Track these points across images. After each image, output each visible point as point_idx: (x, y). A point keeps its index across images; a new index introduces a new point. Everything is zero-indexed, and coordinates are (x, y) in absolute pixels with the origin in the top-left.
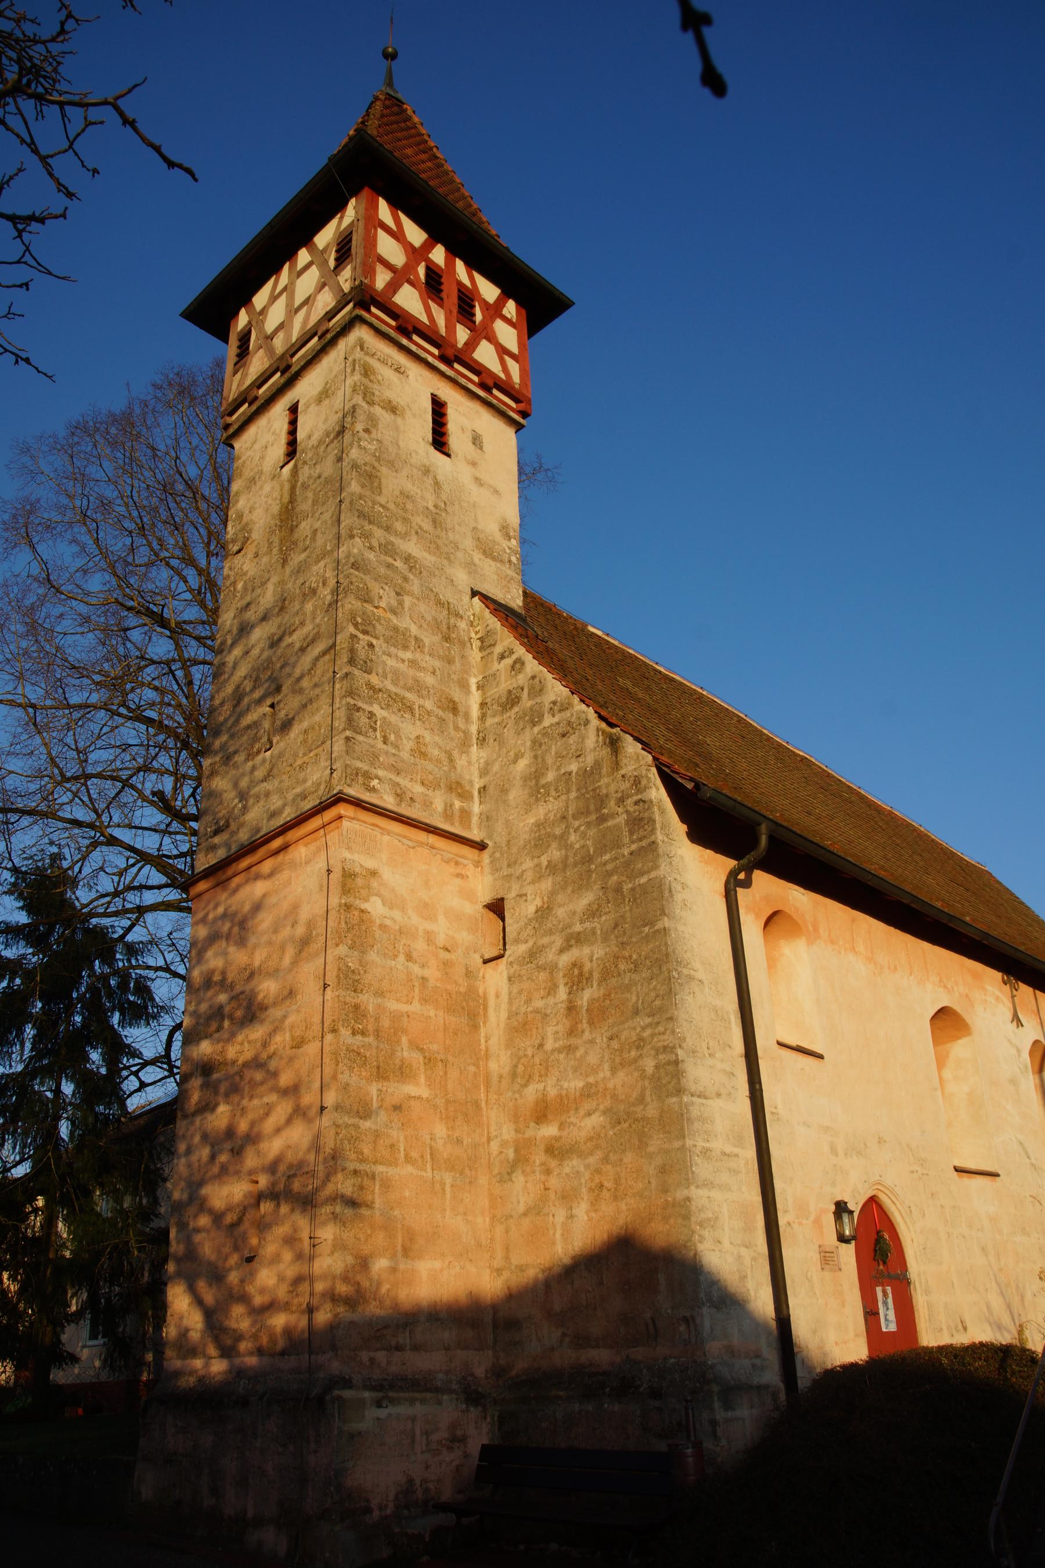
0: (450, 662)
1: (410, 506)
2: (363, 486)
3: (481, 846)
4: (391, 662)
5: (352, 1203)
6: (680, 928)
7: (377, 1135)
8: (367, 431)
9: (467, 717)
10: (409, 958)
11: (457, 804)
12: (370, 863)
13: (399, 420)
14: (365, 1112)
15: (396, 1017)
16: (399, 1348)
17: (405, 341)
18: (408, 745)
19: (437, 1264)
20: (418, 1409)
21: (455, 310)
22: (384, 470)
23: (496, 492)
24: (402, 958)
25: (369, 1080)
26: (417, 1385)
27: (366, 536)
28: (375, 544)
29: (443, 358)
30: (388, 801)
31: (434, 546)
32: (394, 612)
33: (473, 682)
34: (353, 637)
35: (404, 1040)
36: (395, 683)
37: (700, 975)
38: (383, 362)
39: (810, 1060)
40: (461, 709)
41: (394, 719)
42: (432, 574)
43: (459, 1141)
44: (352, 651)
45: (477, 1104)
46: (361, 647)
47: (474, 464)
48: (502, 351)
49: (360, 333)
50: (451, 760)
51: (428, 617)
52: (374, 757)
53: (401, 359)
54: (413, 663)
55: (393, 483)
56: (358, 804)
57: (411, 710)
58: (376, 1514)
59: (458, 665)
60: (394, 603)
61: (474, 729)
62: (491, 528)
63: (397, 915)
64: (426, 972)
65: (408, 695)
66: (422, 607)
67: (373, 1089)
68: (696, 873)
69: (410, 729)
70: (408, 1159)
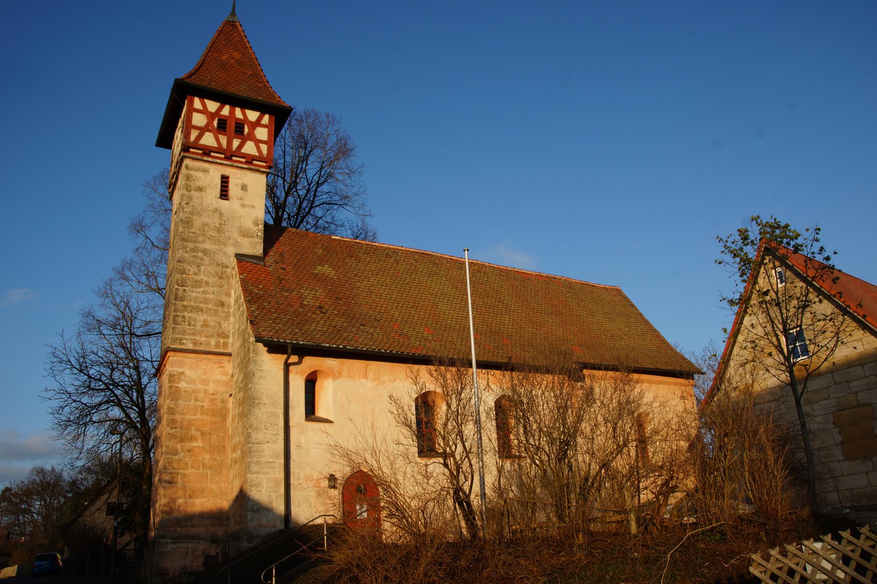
0: (222, 286)
1: (206, 228)
2: (184, 228)
3: (230, 355)
4: (193, 294)
5: (170, 482)
6: (256, 386)
7: (180, 460)
8: (187, 204)
9: (229, 307)
10: (196, 400)
11: (222, 341)
12: (181, 370)
13: (203, 193)
14: (175, 453)
15: (189, 421)
16: (186, 526)
17: (206, 158)
18: (199, 324)
19: (203, 500)
20: (190, 545)
21: (233, 133)
22: (194, 217)
23: (253, 207)
24: (193, 400)
25: (177, 443)
26: (195, 538)
27: (184, 248)
28: (188, 249)
29: (226, 158)
30: (190, 346)
31: (218, 241)
32: (196, 274)
33: (233, 292)
34: (177, 289)
35: (193, 428)
36: (195, 302)
37: (266, 401)
38: (197, 170)
39: (325, 425)
40: (226, 304)
41: (193, 315)
42: (215, 253)
43: (215, 459)
44: (176, 295)
45: (224, 447)
46: (180, 294)
47: (241, 199)
48: (258, 142)
49: (187, 162)
50: (220, 324)
51: (212, 272)
52: (184, 332)
53: (206, 165)
54: (204, 292)
55: (198, 222)
56: (175, 350)
57: (202, 310)
58: (171, 575)
59: (226, 287)
60: (196, 271)
61: (232, 310)
62: (248, 224)
63: (192, 386)
64: (204, 404)
65: (201, 305)
66: (209, 269)
67: (179, 446)
68: (271, 365)
69: (201, 318)
70: (192, 467)
